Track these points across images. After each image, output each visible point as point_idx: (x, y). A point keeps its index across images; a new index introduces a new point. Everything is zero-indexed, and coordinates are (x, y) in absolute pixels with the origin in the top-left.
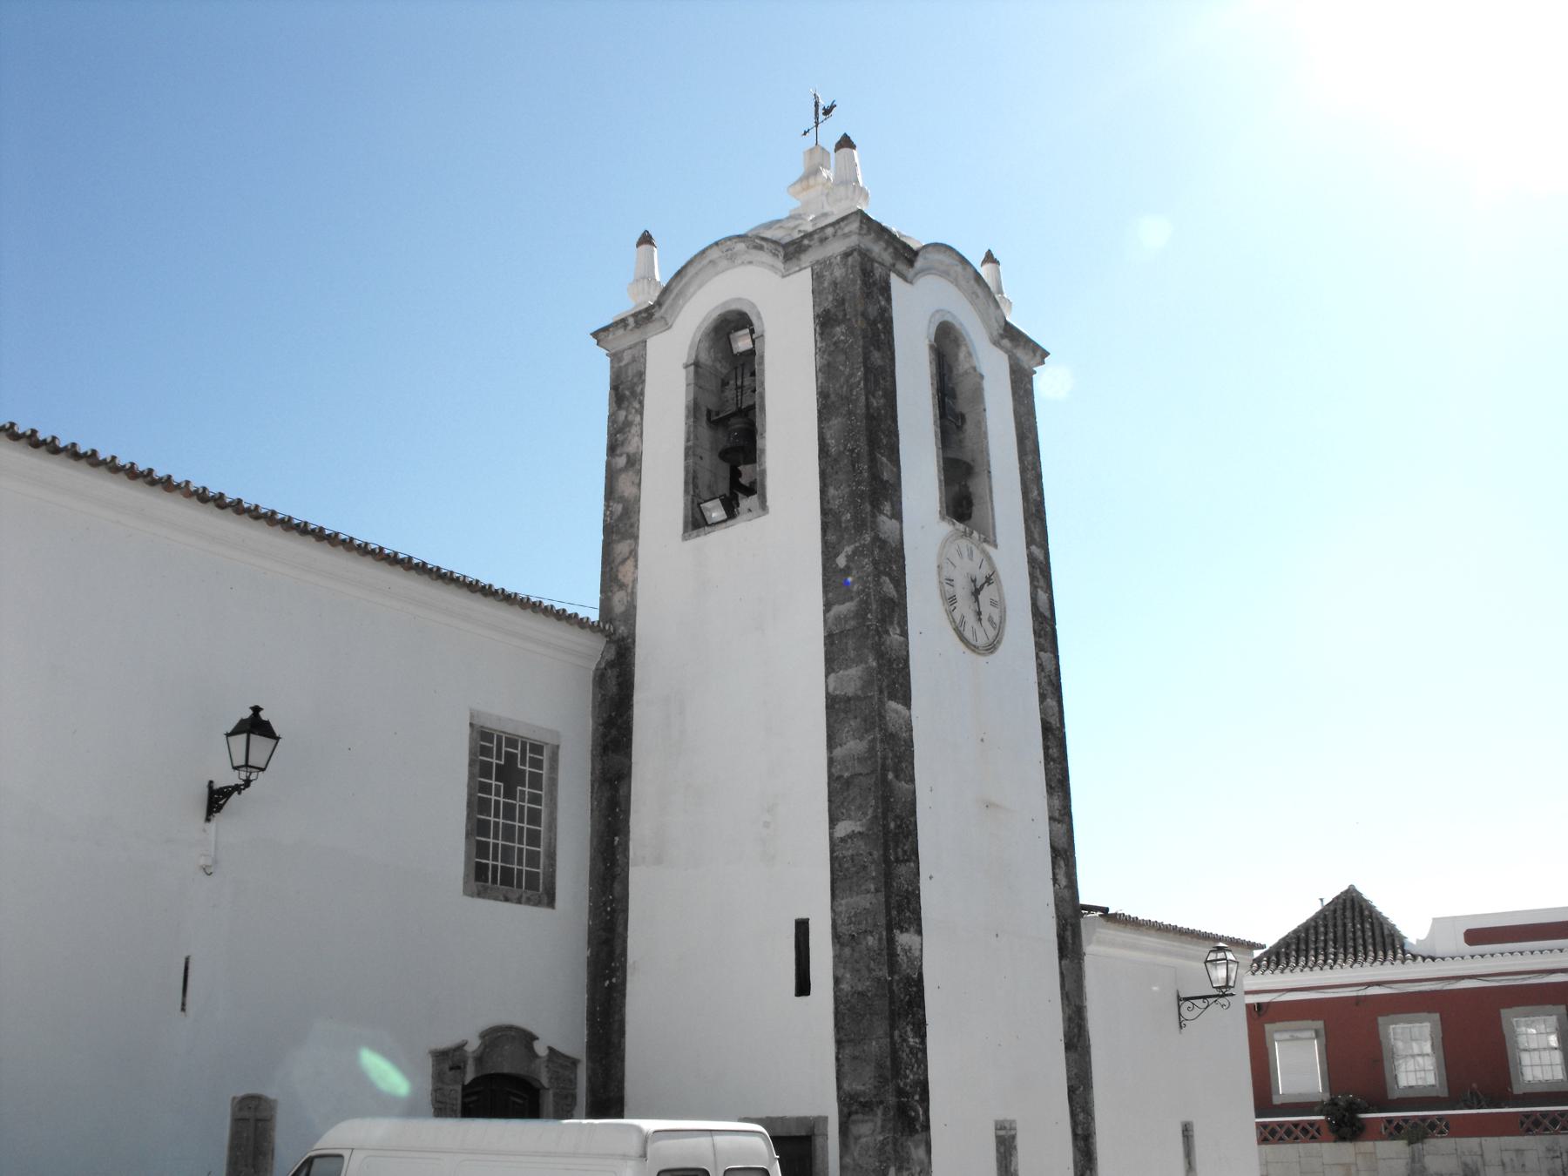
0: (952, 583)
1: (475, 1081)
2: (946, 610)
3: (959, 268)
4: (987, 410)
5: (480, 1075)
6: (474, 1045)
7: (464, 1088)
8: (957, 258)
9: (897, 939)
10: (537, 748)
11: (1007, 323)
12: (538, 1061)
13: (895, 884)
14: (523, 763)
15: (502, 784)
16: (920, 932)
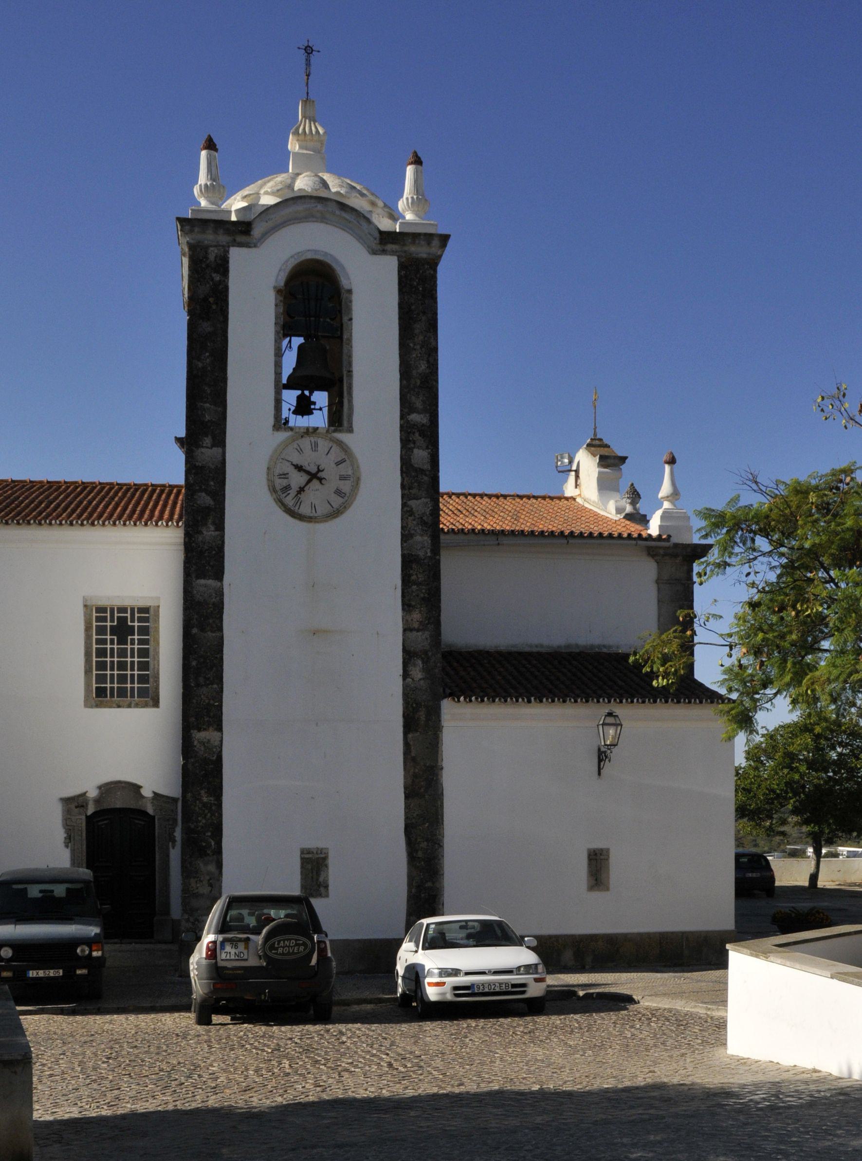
0: (287, 476)
1: (94, 814)
2: (274, 499)
3: (320, 207)
4: (353, 320)
5: (99, 809)
6: (93, 793)
7: (87, 817)
8: (313, 201)
9: (193, 735)
10: (145, 610)
11: (381, 233)
12: (144, 800)
13: (194, 701)
14: (133, 621)
15: (115, 637)
16: (220, 729)
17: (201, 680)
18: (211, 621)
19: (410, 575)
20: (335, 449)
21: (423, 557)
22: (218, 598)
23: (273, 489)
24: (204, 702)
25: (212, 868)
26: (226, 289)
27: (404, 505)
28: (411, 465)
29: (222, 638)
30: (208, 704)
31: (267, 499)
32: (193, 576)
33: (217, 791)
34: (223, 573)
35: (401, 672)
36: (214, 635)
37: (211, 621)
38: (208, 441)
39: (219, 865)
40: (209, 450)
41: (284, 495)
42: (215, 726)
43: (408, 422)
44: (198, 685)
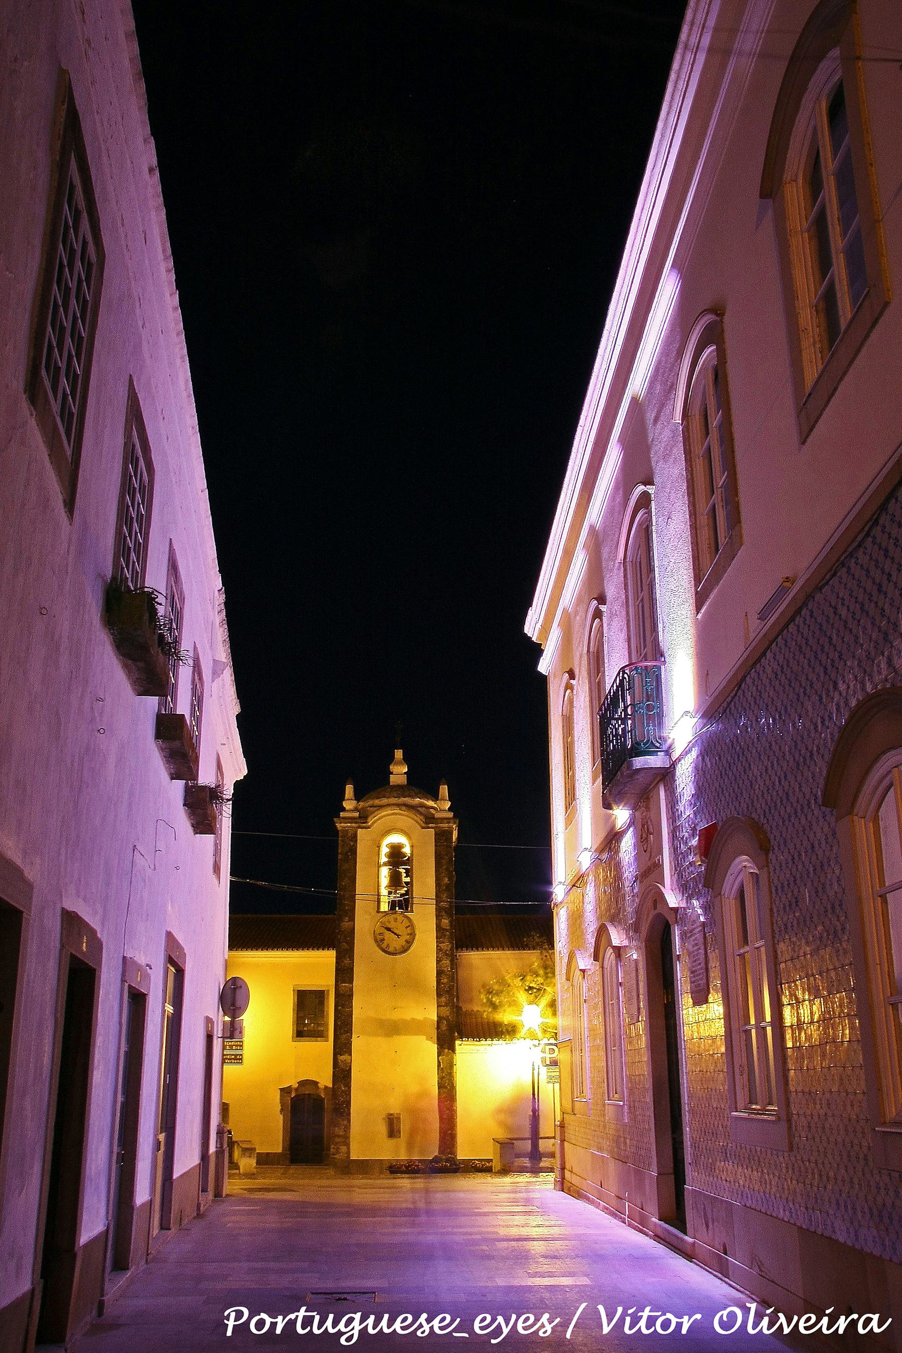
7: (292, 1099)
20: (406, 920)
23: (376, 940)
25: (345, 1122)
26: (356, 848)
29: (352, 1011)
31: (372, 942)
33: (348, 1085)
38: (347, 919)
39: (349, 1121)
43: (439, 907)
44: (340, 1034)
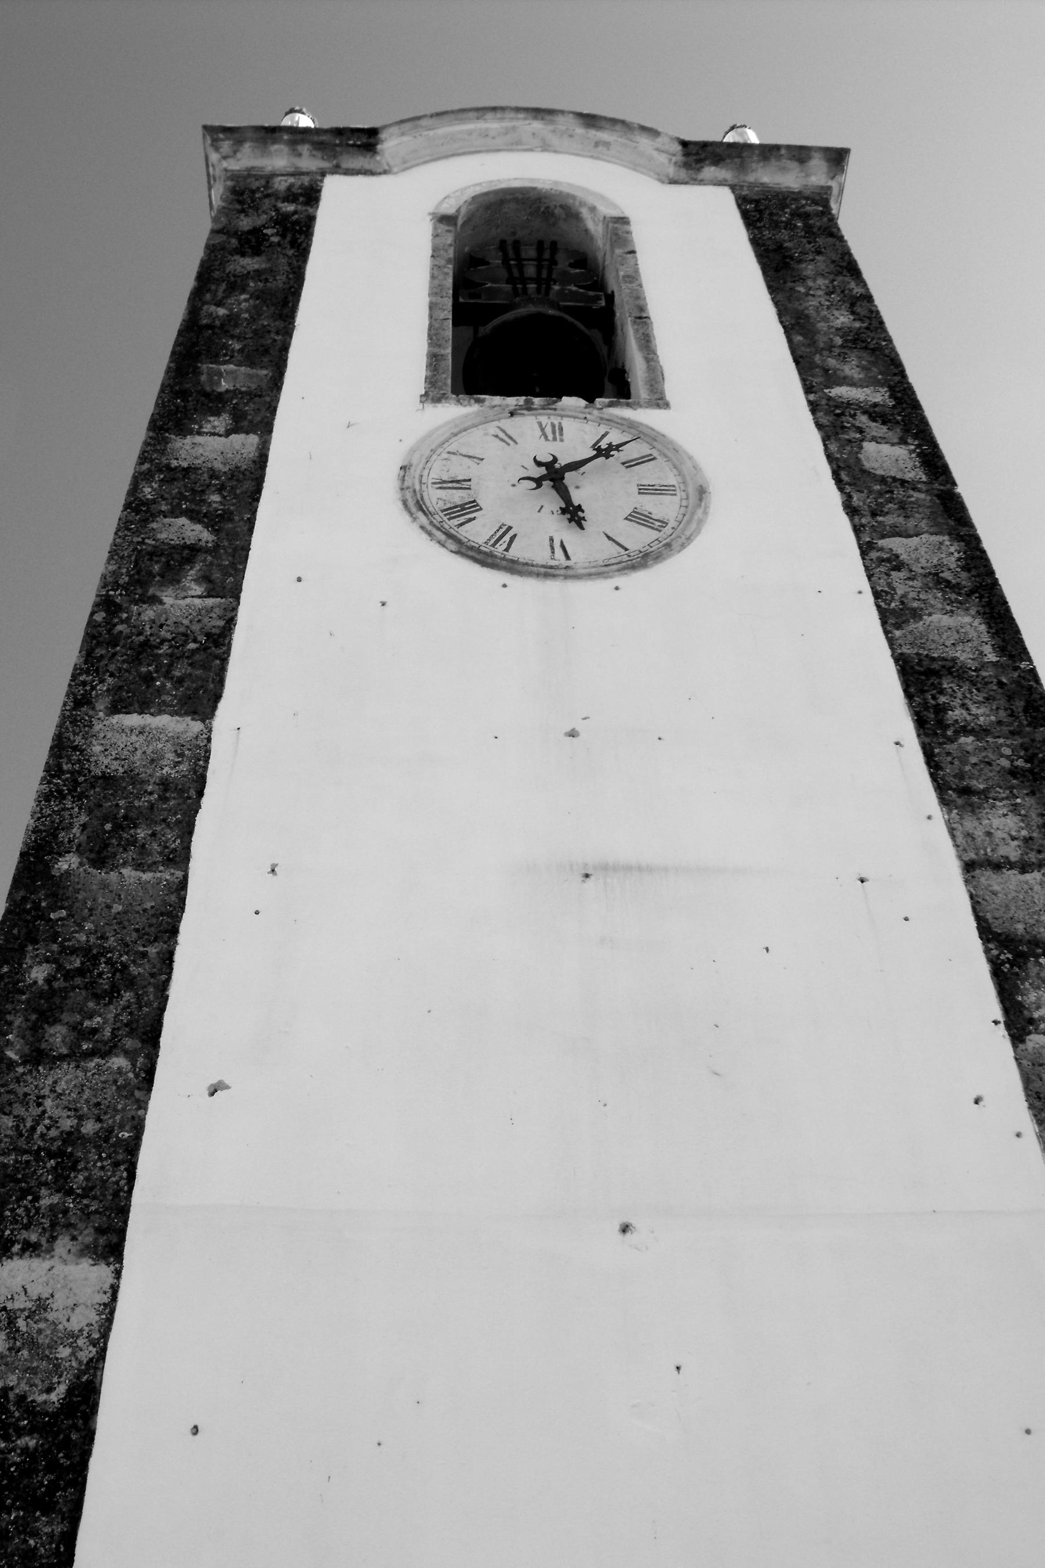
0: (465, 484)
3: (537, 125)
8: (521, 115)
17: (57, 1036)
18: (142, 833)
19: (941, 710)
21: (973, 665)
22: (184, 767)
24: (55, 1121)
27: (865, 550)
28: (864, 472)
30: (71, 1137)
32: (101, 705)
34: (217, 697)
35: (996, 1011)
36: (147, 876)
37: (142, 833)
40: (223, 439)
41: (456, 522)
42: (87, 1236)
